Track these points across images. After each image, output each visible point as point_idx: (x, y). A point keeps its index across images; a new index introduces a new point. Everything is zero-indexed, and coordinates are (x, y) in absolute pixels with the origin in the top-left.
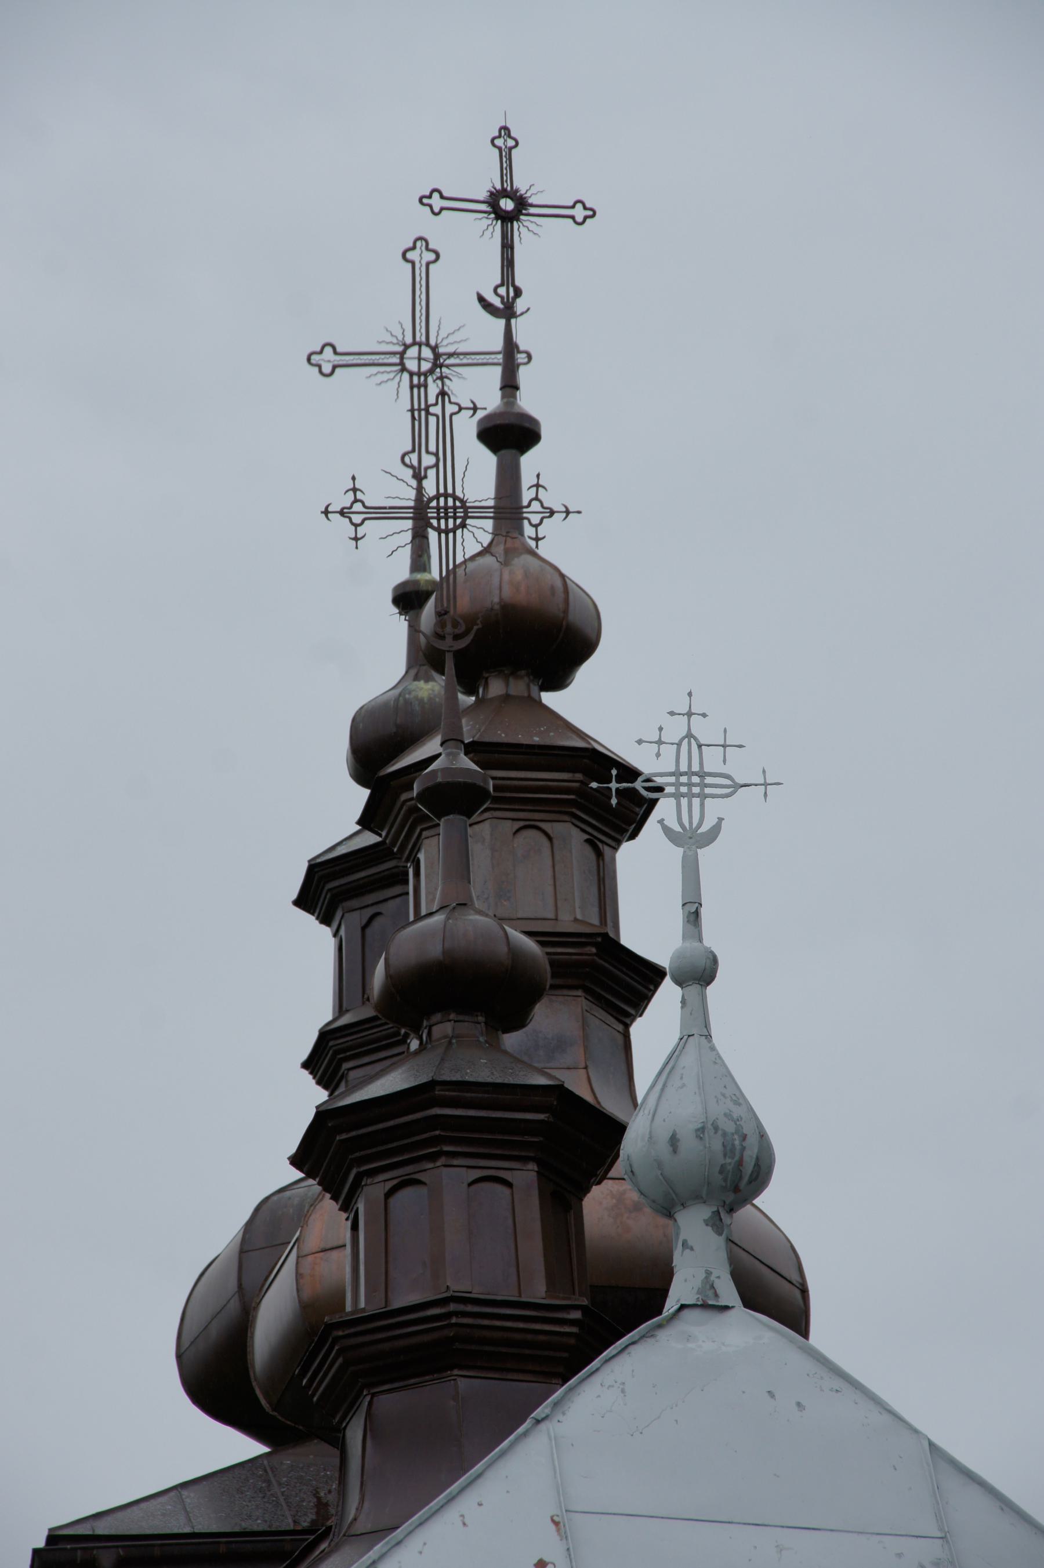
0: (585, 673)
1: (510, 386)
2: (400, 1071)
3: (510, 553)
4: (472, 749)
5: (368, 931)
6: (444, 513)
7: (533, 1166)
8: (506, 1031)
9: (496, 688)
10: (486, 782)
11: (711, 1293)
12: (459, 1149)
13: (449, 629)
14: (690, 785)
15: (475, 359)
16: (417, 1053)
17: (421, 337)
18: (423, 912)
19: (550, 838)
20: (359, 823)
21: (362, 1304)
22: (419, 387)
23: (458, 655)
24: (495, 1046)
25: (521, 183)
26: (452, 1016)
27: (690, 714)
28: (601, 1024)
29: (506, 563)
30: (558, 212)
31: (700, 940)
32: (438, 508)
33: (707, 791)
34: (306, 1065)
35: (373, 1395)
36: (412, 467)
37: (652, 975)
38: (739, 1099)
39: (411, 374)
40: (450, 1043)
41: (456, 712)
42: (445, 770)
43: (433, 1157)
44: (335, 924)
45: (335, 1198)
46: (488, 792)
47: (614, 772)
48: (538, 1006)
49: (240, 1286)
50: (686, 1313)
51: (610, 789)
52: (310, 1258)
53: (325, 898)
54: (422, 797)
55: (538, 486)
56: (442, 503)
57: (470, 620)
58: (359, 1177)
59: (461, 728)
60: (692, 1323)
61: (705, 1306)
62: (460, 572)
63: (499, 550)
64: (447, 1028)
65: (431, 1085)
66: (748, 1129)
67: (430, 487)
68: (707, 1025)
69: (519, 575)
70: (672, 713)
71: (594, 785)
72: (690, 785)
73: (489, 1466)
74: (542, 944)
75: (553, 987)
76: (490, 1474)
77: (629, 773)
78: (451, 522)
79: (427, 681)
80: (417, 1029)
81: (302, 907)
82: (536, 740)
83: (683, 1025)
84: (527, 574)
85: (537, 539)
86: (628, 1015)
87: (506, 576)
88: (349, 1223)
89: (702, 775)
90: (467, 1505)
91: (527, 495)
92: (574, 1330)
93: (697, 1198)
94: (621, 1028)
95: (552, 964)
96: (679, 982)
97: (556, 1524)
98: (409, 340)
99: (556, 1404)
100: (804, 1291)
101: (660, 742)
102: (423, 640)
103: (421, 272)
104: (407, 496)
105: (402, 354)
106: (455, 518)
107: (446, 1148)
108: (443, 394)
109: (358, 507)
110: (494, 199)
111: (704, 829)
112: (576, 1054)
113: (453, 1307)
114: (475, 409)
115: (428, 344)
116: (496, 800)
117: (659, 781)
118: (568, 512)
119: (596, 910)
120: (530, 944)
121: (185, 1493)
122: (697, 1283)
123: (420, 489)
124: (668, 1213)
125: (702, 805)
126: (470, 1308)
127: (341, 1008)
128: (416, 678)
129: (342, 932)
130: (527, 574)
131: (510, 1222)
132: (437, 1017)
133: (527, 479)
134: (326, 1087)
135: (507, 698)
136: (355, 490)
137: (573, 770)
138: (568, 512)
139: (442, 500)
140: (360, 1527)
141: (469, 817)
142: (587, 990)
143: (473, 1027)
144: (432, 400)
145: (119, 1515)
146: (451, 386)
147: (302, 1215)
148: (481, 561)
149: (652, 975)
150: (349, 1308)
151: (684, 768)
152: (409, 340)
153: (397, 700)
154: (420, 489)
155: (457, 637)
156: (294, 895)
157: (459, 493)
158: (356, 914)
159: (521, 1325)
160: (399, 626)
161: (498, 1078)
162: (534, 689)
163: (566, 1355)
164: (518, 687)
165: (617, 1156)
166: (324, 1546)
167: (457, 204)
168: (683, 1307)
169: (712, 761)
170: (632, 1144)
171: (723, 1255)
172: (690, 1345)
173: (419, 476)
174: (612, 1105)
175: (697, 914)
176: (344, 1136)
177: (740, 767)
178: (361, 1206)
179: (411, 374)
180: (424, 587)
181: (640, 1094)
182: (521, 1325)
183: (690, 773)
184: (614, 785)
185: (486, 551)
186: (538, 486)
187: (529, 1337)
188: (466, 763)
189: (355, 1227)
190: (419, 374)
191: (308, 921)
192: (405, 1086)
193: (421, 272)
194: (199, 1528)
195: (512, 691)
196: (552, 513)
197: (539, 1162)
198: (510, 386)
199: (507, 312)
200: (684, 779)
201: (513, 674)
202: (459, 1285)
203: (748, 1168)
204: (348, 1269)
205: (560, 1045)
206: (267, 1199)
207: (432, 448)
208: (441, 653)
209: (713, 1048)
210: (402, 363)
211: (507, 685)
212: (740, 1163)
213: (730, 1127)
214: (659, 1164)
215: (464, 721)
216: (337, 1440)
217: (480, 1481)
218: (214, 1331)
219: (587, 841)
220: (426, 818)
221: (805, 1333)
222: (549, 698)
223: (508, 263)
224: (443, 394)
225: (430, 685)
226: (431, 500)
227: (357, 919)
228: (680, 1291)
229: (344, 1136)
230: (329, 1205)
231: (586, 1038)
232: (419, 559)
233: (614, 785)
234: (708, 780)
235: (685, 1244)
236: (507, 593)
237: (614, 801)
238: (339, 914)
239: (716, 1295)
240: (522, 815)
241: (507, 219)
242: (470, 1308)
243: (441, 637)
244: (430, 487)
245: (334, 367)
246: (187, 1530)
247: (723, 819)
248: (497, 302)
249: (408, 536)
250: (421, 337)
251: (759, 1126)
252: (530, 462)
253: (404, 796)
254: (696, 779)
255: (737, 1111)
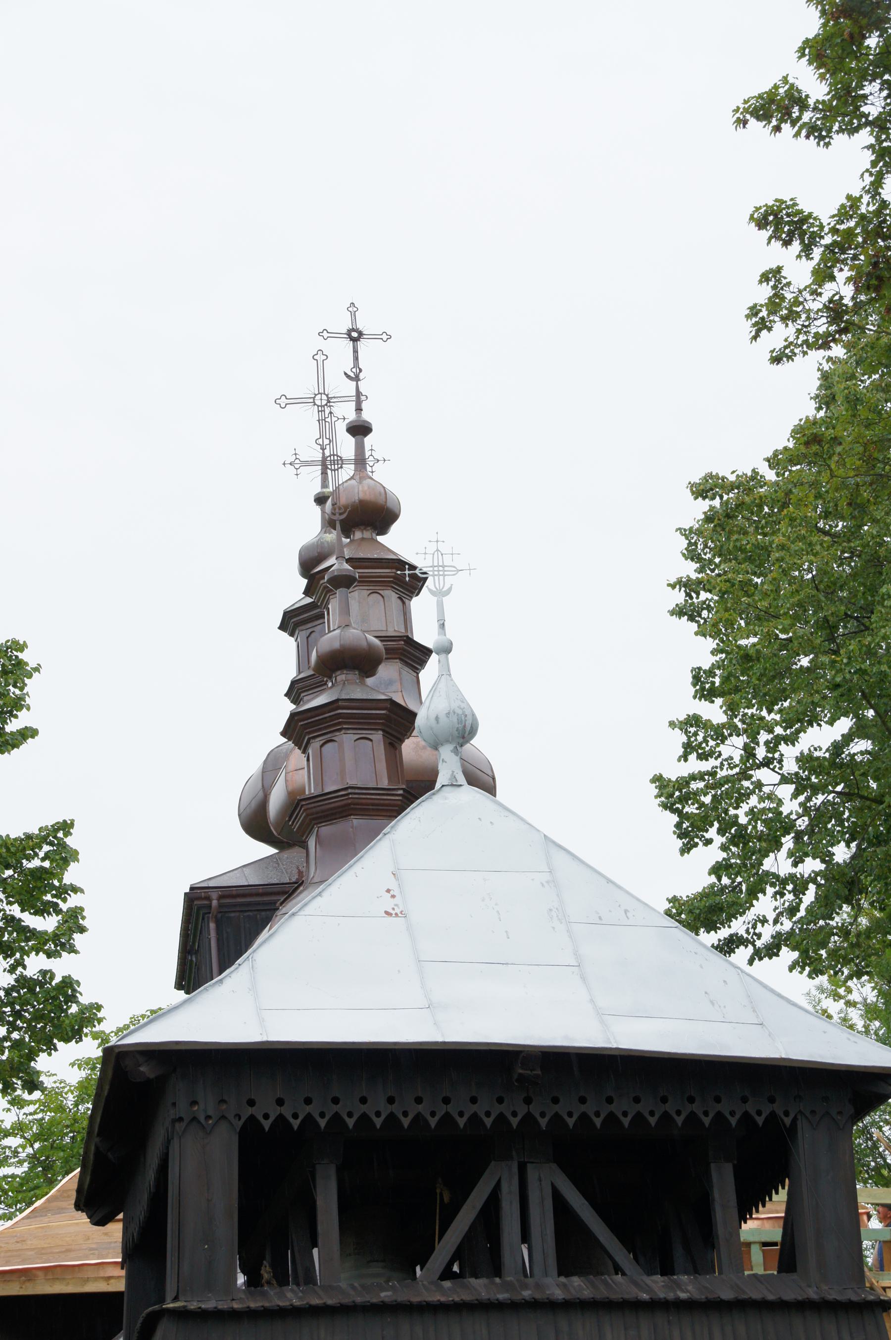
0: (394, 528)
1: (359, 409)
2: (325, 695)
3: (362, 479)
4: (349, 561)
5: (309, 639)
6: (333, 462)
7: (380, 732)
8: (368, 677)
9: (358, 535)
10: (355, 574)
11: (454, 780)
12: (350, 727)
13: (337, 510)
14: (439, 571)
15: (343, 399)
16: (331, 687)
17: (321, 391)
18: (332, 629)
19: (383, 597)
20: (304, 593)
21: (313, 791)
22: (321, 411)
23: (342, 522)
24: (363, 683)
25: (360, 326)
26: (345, 672)
27: (437, 541)
28: (407, 673)
29: (360, 483)
30: (375, 337)
31: (445, 635)
32: (331, 461)
33: (446, 573)
34: (286, 695)
35: (319, 827)
36: (320, 445)
37: (426, 652)
38: (463, 700)
39: (318, 406)
40: (344, 683)
41: (341, 546)
42: (337, 570)
43: (339, 730)
44: (296, 636)
45: (299, 748)
46: (356, 578)
47: (407, 567)
48: (380, 667)
49: (263, 786)
50: (444, 788)
51: (405, 574)
52: (291, 773)
53: (291, 625)
54: (329, 581)
55: (372, 450)
56: (332, 458)
57: (346, 507)
58: (309, 739)
59: (344, 552)
60: (448, 792)
61: (452, 785)
62: (341, 487)
63: (357, 477)
64: (343, 677)
65: (337, 700)
66: (468, 712)
67: (327, 453)
68: (449, 671)
69: (366, 488)
70: (430, 541)
71: (399, 572)
72: (439, 571)
73: (366, 852)
74: (381, 641)
75: (386, 659)
76: (366, 856)
77: (413, 567)
78: (336, 466)
79: (330, 534)
80: (330, 677)
81: (214, 895)
82: (376, 556)
83: (439, 671)
84: (369, 487)
85: (372, 472)
86: (418, 669)
87: (360, 489)
88: (306, 758)
89: (443, 566)
90: (357, 868)
91: (367, 454)
92: (400, 798)
93: (447, 741)
94: (415, 674)
95: (386, 649)
96: (437, 654)
97: (394, 874)
98: (317, 393)
99: (392, 827)
100: (494, 779)
101: (425, 553)
102: (327, 517)
103: (320, 363)
104: (319, 457)
105: (314, 398)
106: (338, 464)
107: (344, 726)
108: (331, 413)
109: (297, 461)
110: (349, 332)
111: (445, 589)
112: (397, 686)
113: (350, 791)
114: (344, 419)
115: (324, 394)
116: (359, 582)
117: (425, 570)
118: (385, 460)
119: (403, 626)
120: (377, 642)
121: (244, 869)
122: (449, 776)
123: (323, 454)
124: (436, 748)
125: (444, 579)
126: (357, 791)
127: (299, 672)
128: (325, 532)
129: (299, 640)
130: (369, 487)
131: (372, 756)
132: (339, 673)
133: (367, 447)
134: (294, 704)
135: (363, 539)
136: (296, 454)
137: (392, 568)
138: (385, 460)
139: (332, 457)
140: (316, 880)
141: (349, 589)
142: (400, 659)
143: (353, 676)
144: (326, 416)
145: (218, 878)
146: (333, 410)
147: (287, 756)
148: (349, 482)
149: (426, 652)
150: (307, 793)
151: (436, 564)
152: (317, 393)
153: (317, 542)
154: (323, 454)
155: (341, 514)
156: (278, 625)
157: (339, 454)
158: (304, 632)
159: (378, 797)
160: (317, 510)
161: (365, 697)
162: (374, 535)
163: (397, 808)
164: (367, 534)
165: (414, 728)
166: (301, 888)
167: (333, 335)
168: (443, 786)
169: (447, 561)
170: (419, 721)
171: (459, 764)
172: (447, 801)
173: (323, 449)
174: (412, 706)
175: (443, 624)
176: (302, 723)
177: (459, 563)
178: (310, 751)
179: (318, 406)
180: (327, 495)
181: (423, 699)
182: (378, 797)
183: (438, 566)
184: (407, 572)
185: (352, 478)
186: (372, 450)
187: (382, 802)
188: (347, 566)
189: (308, 760)
190: (321, 406)
191: (285, 635)
192: (327, 701)
193: (320, 363)
194: (251, 883)
195: (365, 536)
196: (378, 461)
197: (383, 731)
198: (359, 409)
199: (357, 379)
200: (436, 569)
201: (365, 529)
202: (352, 782)
203: (468, 728)
204: (306, 777)
205: (390, 682)
206: (269, 755)
207: (328, 437)
208: (335, 521)
209: (452, 680)
210: (314, 402)
211: (363, 533)
212: (465, 726)
213: (460, 712)
214: (431, 728)
215: (345, 550)
216: (304, 845)
217: (362, 859)
218: (253, 805)
219: (399, 598)
220: (331, 590)
221: (495, 795)
222: (380, 538)
223: (356, 358)
224: (331, 413)
225: (331, 535)
226: (327, 457)
227: (305, 634)
228: (441, 780)
229: (302, 723)
230: (298, 752)
231: (401, 679)
232: (324, 484)
233: (407, 572)
234: (446, 569)
235: (443, 761)
236: (362, 496)
237: (407, 579)
238: (297, 632)
239: (456, 780)
240: (371, 588)
241: (354, 340)
242: (357, 791)
243: (334, 514)
244: (327, 453)
245: (286, 404)
246: (246, 884)
247: (669, 585)
248: (352, 375)
249: (320, 472)
250: (321, 391)
251: (472, 711)
252: (368, 440)
253: (322, 582)
254: (441, 568)
255: (463, 705)
